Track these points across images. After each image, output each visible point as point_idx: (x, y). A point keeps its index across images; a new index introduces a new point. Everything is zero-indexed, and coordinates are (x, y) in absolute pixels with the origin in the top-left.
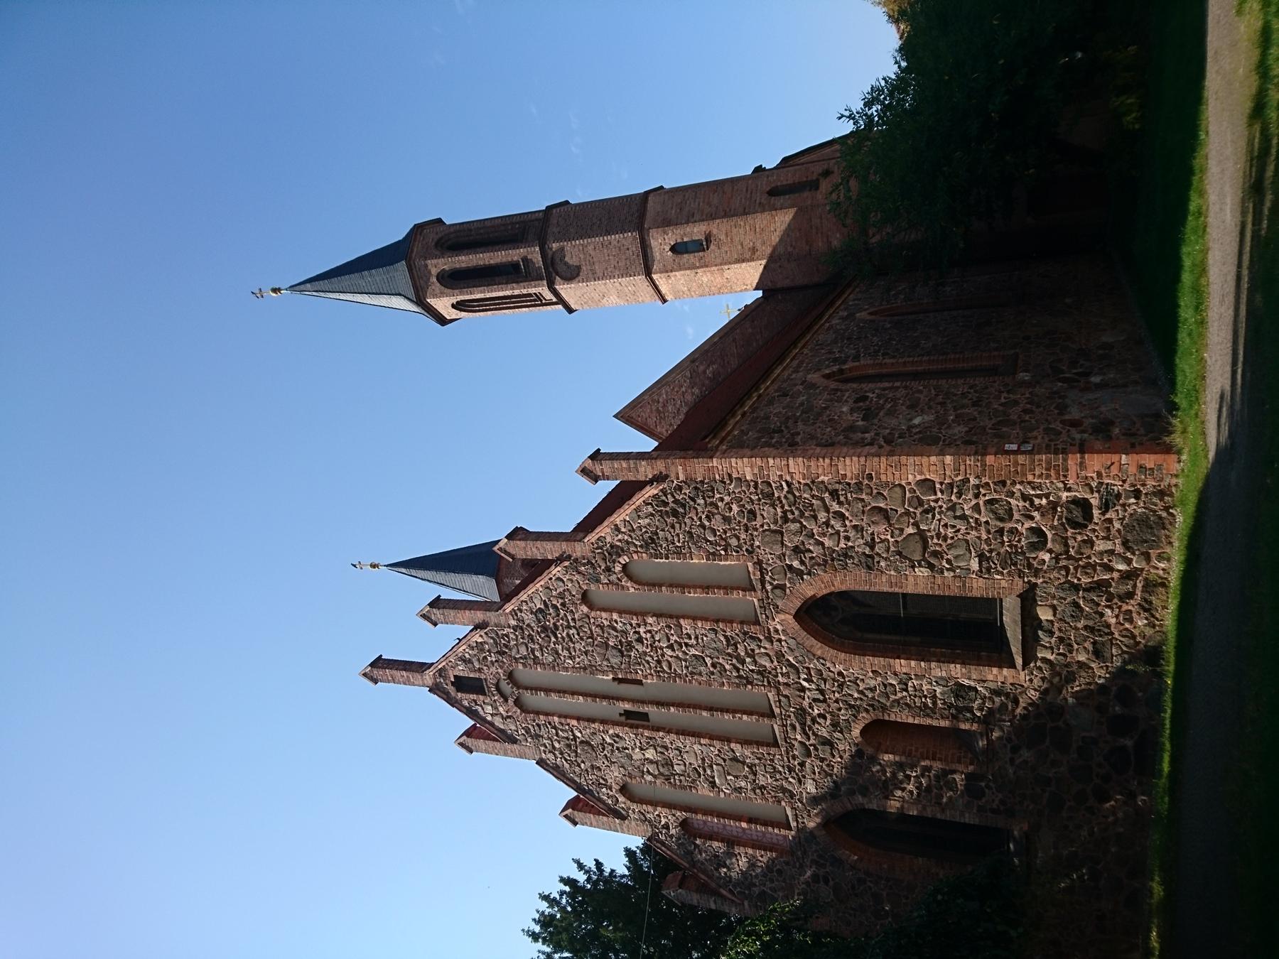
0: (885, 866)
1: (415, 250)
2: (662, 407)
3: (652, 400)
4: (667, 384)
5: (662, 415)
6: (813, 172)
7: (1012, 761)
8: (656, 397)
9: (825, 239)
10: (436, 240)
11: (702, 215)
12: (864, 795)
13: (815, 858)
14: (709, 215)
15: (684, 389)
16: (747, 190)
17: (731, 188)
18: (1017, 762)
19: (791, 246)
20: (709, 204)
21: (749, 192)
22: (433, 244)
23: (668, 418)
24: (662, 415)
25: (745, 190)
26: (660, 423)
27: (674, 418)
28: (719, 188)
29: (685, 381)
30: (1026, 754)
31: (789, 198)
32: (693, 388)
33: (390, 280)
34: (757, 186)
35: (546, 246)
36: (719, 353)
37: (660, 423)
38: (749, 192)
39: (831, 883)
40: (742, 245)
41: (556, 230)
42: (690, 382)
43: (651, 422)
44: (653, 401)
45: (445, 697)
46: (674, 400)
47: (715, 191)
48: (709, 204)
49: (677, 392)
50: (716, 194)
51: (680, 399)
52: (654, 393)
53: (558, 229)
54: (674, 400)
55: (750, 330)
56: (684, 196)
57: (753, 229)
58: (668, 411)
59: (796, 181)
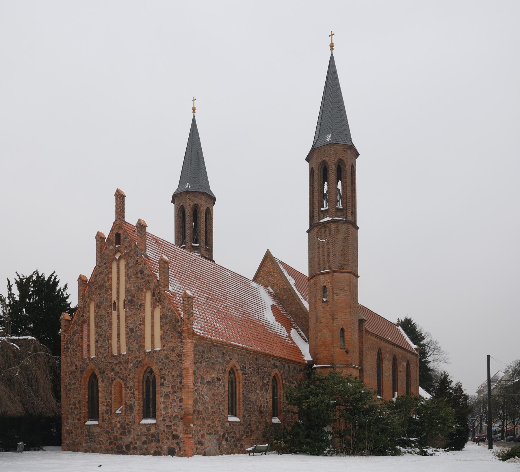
0: (83, 387)
1: (339, 147)
2: (271, 274)
3: (274, 269)
4: (281, 277)
5: (268, 274)
6: (349, 346)
7: (116, 421)
8: (276, 271)
9: (321, 352)
10: (343, 159)
11: (336, 300)
12: (102, 381)
13: (82, 366)
14: (336, 303)
15: (279, 285)
16: (345, 319)
17: (347, 311)
18: (116, 423)
19: (320, 338)
20: (342, 302)
21: (344, 320)
22: (341, 157)
23: (267, 277)
24: (268, 274)
25: (346, 318)
26: (265, 273)
27: (267, 280)
28: (349, 306)
29: (282, 286)
30: (118, 425)
31: (339, 337)
32: (279, 290)
33: (326, 130)
34: (346, 323)
35: (332, 223)
36: (293, 302)
37: (265, 273)
38: (344, 320)
39: (76, 370)
40: (323, 318)
41: (339, 228)
42: (281, 288)
43: (265, 269)
44: (274, 270)
45: (113, 229)
46: (274, 280)
47: (347, 304)
48: (342, 302)
49: (278, 282)
50: (346, 305)
51: (275, 283)
52: (278, 270)
53: (340, 229)
54: (274, 280)
55: (301, 316)
56: (347, 291)
57: (328, 322)
58: (270, 277)
59: (346, 339)
